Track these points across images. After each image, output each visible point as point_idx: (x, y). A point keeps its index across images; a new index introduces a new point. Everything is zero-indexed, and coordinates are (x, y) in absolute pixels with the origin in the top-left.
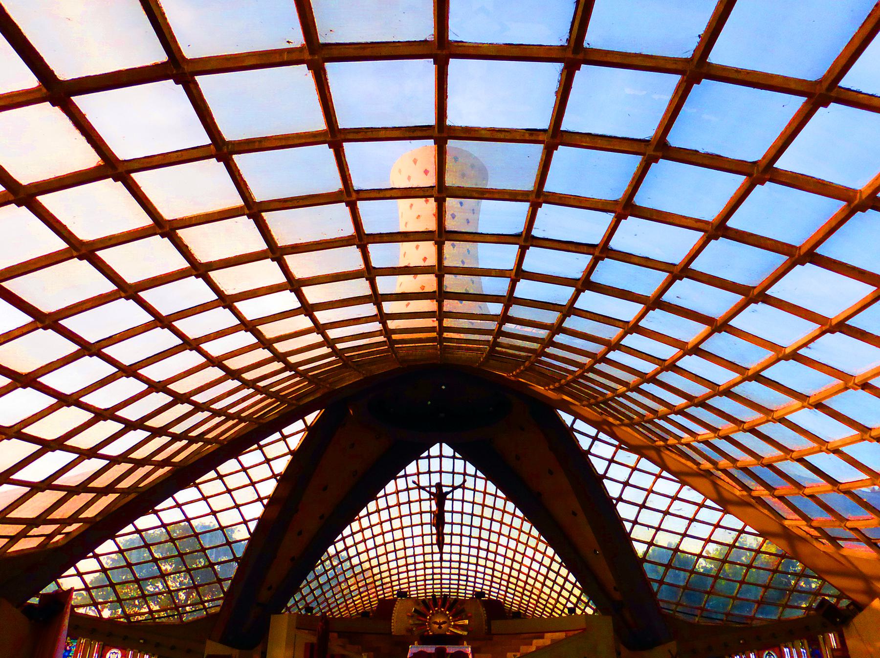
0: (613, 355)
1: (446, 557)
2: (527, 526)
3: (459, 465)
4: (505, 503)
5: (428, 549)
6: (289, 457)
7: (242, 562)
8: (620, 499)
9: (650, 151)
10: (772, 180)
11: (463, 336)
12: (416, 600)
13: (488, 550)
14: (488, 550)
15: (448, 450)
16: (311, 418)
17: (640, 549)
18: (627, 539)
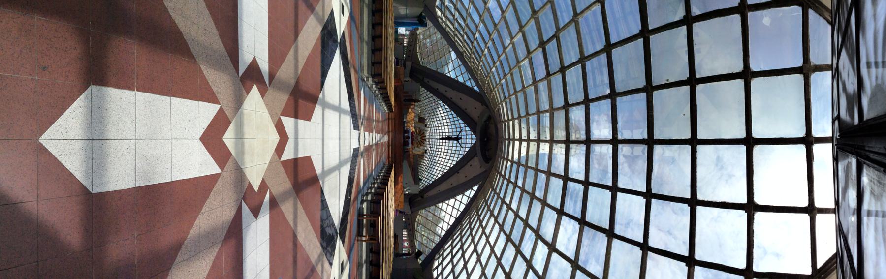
1: (438, 141)
2: (448, 168)
4: (340, 104)
6: (471, 86)
7: (436, 72)
9: (476, 167)
10: (573, 270)
12: (424, 130)
13: (440, 155)
14: (440, 155)
15: (474, 141)
16: (476, 88)
17: (440, 205)
18: (443, 201)
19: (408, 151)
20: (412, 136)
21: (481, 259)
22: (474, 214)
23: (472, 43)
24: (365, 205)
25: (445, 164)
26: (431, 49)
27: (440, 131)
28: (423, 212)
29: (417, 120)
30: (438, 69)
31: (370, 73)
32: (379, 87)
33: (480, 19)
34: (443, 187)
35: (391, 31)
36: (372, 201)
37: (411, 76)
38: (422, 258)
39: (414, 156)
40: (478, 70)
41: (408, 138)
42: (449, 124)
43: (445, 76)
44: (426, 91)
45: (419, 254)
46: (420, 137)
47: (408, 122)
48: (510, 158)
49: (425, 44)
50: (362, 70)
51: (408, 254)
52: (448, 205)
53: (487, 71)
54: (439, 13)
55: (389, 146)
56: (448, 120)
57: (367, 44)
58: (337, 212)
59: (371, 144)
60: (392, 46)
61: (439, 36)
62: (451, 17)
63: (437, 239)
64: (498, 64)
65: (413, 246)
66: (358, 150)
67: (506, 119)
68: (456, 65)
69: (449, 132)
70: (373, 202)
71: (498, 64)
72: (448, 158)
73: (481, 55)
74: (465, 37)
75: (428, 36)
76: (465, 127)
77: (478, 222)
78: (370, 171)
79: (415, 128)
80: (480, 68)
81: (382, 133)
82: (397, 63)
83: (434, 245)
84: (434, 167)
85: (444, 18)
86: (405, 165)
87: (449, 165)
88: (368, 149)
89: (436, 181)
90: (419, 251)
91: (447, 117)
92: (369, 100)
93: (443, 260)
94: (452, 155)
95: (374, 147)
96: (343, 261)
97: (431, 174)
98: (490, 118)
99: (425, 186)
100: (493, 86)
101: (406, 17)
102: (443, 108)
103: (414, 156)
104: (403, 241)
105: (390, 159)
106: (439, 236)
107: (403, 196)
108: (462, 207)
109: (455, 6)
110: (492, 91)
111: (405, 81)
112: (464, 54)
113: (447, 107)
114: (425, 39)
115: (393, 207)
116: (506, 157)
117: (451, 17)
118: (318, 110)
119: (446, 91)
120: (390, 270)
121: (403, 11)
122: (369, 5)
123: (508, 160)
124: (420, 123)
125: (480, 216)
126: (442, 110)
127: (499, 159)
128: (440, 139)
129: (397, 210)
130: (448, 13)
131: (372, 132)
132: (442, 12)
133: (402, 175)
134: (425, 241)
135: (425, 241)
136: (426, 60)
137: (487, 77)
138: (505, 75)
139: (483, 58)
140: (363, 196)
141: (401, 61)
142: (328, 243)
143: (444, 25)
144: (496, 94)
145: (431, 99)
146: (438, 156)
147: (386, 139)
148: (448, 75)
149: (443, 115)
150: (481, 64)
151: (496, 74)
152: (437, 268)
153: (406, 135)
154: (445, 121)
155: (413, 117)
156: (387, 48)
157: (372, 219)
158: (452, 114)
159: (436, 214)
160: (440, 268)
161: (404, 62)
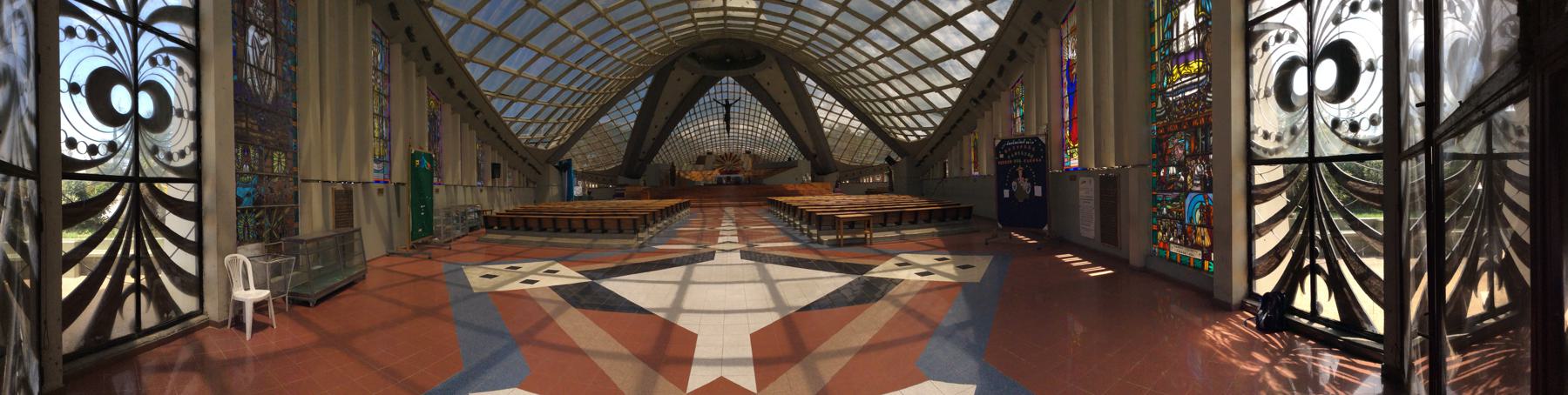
0: (814, 42)
1: (731, 134)
2: (772, 119)
3: (738, 87)
5: (722, 131)
8: (819, 107)
9: (769, 76)
11: (713, 22)
12: (716, 156)
16: (649, 81)
18: (821, 127)
19: (749, 178)
20: (726, 172)
21: (899, 73)
22: (838, 80)
23: (585, 93)
24: (825, 238)
25: (766, 123)
26: (601, 151)
27: (717, 132)
28: (836, 155)
29: (702, 166)
30: (625, 141)
31: (632, 235)
32: (651, 223)
33: (554, 86)
34: (800, 125)
35: (579, 205)
36: (819, 228)
37: (639, 178)
38: (894, 156)
39: (755, 169)
40: (621, 80)
41: (728, 179)
42: (705, 119)
43: (634, 130)
44: (658, 156)
45: (889, 159)
46: (728, 161)
47: (705, 179)
48: (753, 15)
49: (594, 160)
50: (628, 247)
51: (890, 175)
52: (826, 119)
53: (621, 66)
54: (554, 144)
55: (742, 206)
56: (700, 121)
57: (595, 239)
58: (832, 280)
59: (736, 233)
60: (597, 204)
61: (581, 142)
62: (557, 128)
63: (872, 136)
64: (608, 50)
65: (882, 169)
66: (745, 252)
67: (691, 25)
68: (618, 114)
69: (718, 119)
70: (820, 226)
71: (608, 50)
72: (756, 120)
73: (599, 78)
74: (579, 105)
75: (583, 156)
76: (709, 94)
77: (850, 73)
78: (777, 232)
79: (714, 169)
80: (618, 77)
81: (722, 216)
82: (620, 196)
83: (879, 140)
84: (771, 140)
85: (559, 138)
86: (769, 181)
87: (768, 118)
88: (743, 236)
89: (791, 137)
90: (886, 159)
91: (695, 123)
92: (671, 237)
93: (896, 127)
94: (752, 113)
95: (741, 228)
96: (897, 264)
97: (781, 143)
98: (693, 55)
99: (800, 153)
100: (643, 52)
101: (561, 186)
102: (681, 129)
103: (755, 169)
104: (874, 182)
105: (762, 203)
106: (869, 132)
107: (815, 184)
108: (829, 98)
109: (543, 124)
110: (651, 54)
111: (645, 184)
112: (601, 103)
113: (679, 124)
114: (587, 162)
115: (829, 197)
116: (753, 23)
117: (557, 128)
118: (684, 321)
119: (656, 127)
120: (908, 198)
121: (554, 191)
122: (548, 236)
123: (757, 20)
124: (706, 163)
125: (842, 72)
126: (684, 131)
127: (757, 35)
128: (728, 132)
129: (834, 192)
130: (552, 133)
131: (719, 231)
132: (553, 140)
133: (785, 185)
134: (875, 151)
135: (875, 151)
136: (615, 157)
137: (630, 65)
138: (623, 35)
139: (603, 74)
140: (813, 242)
141: (618, 190)
142: (873, 291)
143: (568, 136)
144: (655, 47)
145: (669, 148)
146: (754, 134)
147: (730, 210)
148: (632, 125)
149: (692, 130)
150: (611, 76)
151: (625, 51)
152: (906, 136)
153: (724, 181)
154: (701, 126)
155: (698, 172)
156: (600, 210)
157: (842, 226)
158: (690, 115)
159: (838, 137)
160: (906, 132)
161: (618, 186)
